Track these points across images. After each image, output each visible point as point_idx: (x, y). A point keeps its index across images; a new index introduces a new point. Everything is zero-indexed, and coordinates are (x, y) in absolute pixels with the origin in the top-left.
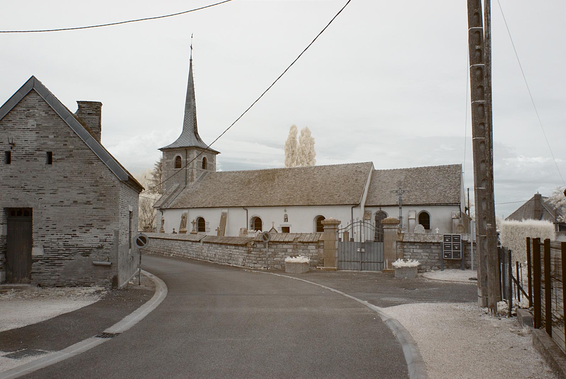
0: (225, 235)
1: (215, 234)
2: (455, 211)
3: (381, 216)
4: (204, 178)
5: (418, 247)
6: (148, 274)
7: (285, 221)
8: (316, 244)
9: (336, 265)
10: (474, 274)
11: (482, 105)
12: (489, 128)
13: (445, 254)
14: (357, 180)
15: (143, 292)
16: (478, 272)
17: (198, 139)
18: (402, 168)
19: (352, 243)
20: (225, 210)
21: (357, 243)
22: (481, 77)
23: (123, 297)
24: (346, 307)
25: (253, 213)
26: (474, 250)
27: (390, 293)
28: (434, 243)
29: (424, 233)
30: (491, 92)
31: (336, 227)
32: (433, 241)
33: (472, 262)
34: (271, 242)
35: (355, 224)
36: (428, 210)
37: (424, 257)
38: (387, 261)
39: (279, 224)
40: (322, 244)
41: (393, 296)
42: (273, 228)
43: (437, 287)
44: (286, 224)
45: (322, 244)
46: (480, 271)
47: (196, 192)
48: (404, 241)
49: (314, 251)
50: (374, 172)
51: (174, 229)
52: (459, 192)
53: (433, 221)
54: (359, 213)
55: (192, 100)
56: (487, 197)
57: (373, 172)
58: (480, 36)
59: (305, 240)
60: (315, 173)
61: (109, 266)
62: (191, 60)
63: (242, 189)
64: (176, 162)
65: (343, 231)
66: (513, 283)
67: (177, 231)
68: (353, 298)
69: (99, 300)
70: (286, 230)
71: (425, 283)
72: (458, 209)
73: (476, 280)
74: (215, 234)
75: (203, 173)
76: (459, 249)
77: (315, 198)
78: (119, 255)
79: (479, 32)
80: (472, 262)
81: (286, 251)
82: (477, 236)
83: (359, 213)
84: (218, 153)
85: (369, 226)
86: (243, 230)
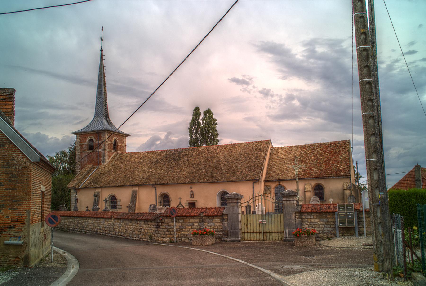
0: (136, 212)
1: (126, 210)
2: (346, 183)
3: (280, 188)
6: (61, 251)
7: (191, 197)
8: (220, 218)
9: (240, 237)
10: (370, 241)
11: (369, 83)
12: (377, 104)
13: (340, 223)
14: (257, 157)
15: (53, 270)
16: (373, 238)
17: (109, 122)
18: (298, 145)
19: (254, 215)
20: (136, 189)
21: (259, 215)
22: (367, 57)
23: (34, 275)
24: (251, 277)
25: (160, 190)
26: (366, 217)
27: (291, 261)
28: (330, 212)
29: (319, 203)
30: (377, 71)
31: (239, 201)
33: (365, 229)
34: (178, 216)
35: (257, 198)
36: (322, 182)
37: (321, 226)
38: (287, 231)
39: (185, 199)
40: (226, 217)
41: (294, 265)
42: (180, 203)
43: (334, 253)
44: (191, 200)
45: (226, 217)
46: (375, 237)
47: (108, 172)
48: (302, 211)
49: (219, 224)
50: (272, 148)
51: (87, 207)
52: (349, 166)
54: (260, 188)
55: (103, 87)
56: (378, 168)
57: (271, 150)
58: (364, 21)
60: (218, 152)
61: (20, 245)
62: (102, 51)
63: (150, 168)
65: (246, 204)
67: (90, 209)
68: (257, 267)
69: (10, 279)
70: (192, 205)
71: (323, 250)
73: (371, 245)
74: (126, 210)
76: (352, 217)
77: (219, 175)
78: (31, 234)
79: (363, 17)
80: (365, 229)
81: (193, 225)
82: (370, 205)
83: (260, 188)
84: (127, 135)
85: (269, 199)
86: (152, 207)
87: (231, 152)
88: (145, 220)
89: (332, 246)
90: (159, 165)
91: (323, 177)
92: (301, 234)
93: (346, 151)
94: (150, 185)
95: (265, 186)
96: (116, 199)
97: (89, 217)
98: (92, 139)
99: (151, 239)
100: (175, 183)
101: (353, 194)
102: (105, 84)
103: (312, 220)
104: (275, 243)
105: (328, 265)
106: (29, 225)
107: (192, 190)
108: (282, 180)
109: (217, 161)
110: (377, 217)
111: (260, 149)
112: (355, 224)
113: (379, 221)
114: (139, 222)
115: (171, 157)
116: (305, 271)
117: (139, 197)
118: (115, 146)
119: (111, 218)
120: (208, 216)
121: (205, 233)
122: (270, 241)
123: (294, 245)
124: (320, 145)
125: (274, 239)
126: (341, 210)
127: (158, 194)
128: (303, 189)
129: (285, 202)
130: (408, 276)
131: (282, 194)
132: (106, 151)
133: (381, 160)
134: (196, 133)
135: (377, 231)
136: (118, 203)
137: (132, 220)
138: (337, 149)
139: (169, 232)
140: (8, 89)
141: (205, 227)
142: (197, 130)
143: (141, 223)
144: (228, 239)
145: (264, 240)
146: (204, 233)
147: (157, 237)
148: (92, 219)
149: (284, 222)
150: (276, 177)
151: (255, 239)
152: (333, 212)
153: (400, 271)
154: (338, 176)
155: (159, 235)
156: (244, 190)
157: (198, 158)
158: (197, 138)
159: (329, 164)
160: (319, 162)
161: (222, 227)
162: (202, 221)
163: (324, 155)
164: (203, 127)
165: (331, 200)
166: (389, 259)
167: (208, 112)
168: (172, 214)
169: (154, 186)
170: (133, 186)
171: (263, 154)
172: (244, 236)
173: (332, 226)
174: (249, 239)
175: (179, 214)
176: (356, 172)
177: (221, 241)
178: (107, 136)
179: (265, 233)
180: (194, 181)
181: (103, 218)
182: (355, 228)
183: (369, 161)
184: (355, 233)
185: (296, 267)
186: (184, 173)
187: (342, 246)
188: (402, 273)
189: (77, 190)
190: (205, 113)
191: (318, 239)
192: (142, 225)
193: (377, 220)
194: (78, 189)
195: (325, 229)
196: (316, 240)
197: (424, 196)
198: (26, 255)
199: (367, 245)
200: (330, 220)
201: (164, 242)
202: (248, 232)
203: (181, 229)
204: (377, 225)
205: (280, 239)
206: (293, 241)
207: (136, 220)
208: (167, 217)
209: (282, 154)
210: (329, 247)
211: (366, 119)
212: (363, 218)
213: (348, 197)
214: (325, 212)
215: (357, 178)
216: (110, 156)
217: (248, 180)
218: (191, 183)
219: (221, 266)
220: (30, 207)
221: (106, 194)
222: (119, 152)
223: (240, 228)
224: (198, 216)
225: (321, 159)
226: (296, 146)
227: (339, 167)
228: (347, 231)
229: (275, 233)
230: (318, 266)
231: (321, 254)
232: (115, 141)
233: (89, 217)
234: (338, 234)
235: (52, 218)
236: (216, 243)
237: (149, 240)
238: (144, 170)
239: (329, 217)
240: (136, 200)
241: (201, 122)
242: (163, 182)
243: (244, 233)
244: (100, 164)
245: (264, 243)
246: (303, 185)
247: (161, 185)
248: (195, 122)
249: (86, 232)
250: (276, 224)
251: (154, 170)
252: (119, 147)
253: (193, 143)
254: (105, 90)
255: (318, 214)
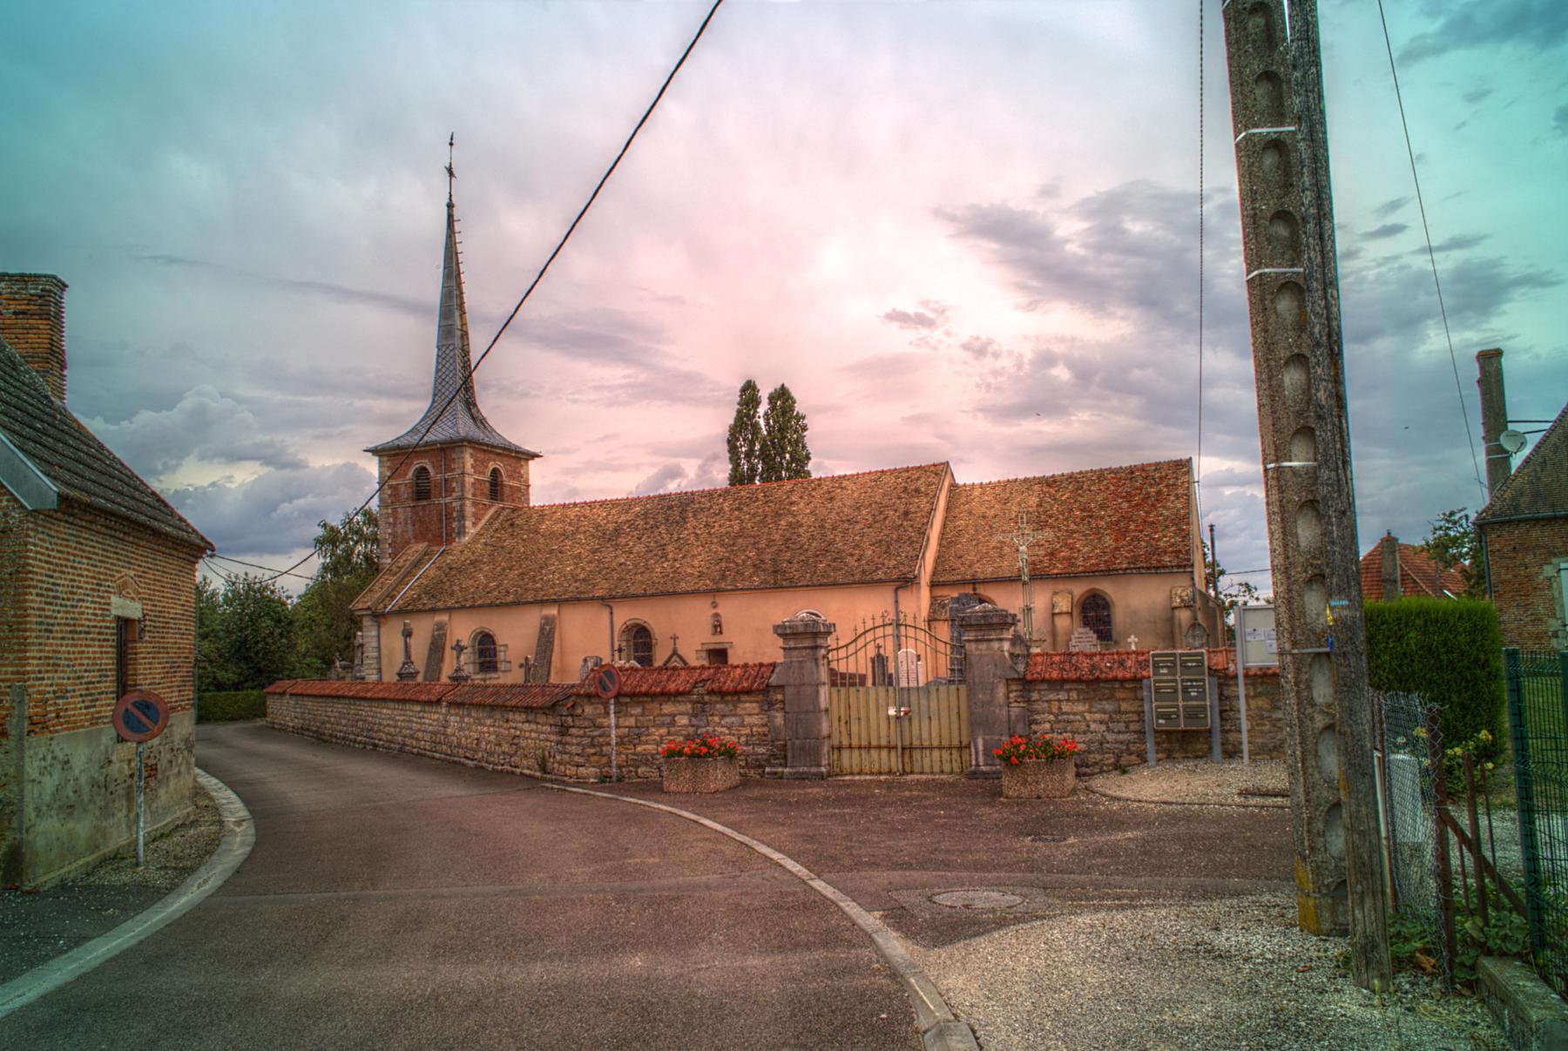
0: (554, 680)
2: (1180, 589)
4: (497, 525)
5: (1074, 695)
7: (715, 633)
8: (760, 697)
9: (824, 762)
14: (906, 513)
20: (552, 611)
25: (625, 615)
26: (1247, 696)
28: (1123, 681)
30: (1317, 64)
31: (820, 642)
32: (1120, 675)
33: (1245, 737)
34: (626, 695)
36: (1107, 587)
37: (1093, 726)
42: (675, 653)
43: (1138, 826)
44: (714, 641)
45: (780, 697)
47: (472, 563)
48: (1029, 677)
49: (755, 720)
50: (954, 486)
52: (1186, 536)
53: (1119, 616)
54: (918, 603)
55: (457, 313)
57: (950, 491)
59: (729, 685)
60: (794, 499)
64: (417, 485)
66: (1454, 854)
70: (719, 655)
71: (1099, 813)
72: (1188, 583)
75: (492, 511)
80: (1245, 737)
81: (673, 723)
84: (534, 456)
86: (590, 665)
87: (831, 499)
88: (528, 709)
89: (1132, 796)
90: (622, 540)
91: (1109, 572)
92: (1023, 756)
93: (1180, 491)
94: (592, 599)
95: (933, 598)
96: (494, 642)
97: (384, 700)
98: (424, 469)
99: (544, 769)
100: (666, 593)
101: (1200, 620)
102: (461, 305)
103: (1065, 707)
104: (940, 786)
105: (1109, 885)
106: (21, 739)
107: (718, 610)
108: (985, 582)
109: (790, 525)
110: (1313, 705)
111: (917, 491)
112: (1212, 719)
113: (1320, 721)
114: (511, 716)
115: (660, 518)
116: (1017, 920)
117: (561, 639)
118: (495, 488)
119: (439, 702)
120: (722, 694)
121: (705, 750)
122: (924, 777)
123: (1001, 794)
124: (1100, 475)
125: (936, 769)
126: (1165, 671)
127: (618, 626)
128: (1040, 609)
129: (973, 646)
130: (1462, 974)
131: (963, 619)
132: (468, 503)
133: (1336, 458)
134: (749, 455)
135: (1311, 762)
136: (501, 656)
137: (493, 708)
138: (1151, 485)
139: (597, 743)
140: (35, 276)
141: (710, 729)
142: (752, 444)
143: (517, 717)
144: (787, 770)
145: (904, 773)
146: (703, 752)
147: (560, 763)
148: (392, 705)
149: (971, 714)
150: (965, 572)
151: (876, 768)
152: (1136, 680)
153: (1418, 945)
154: (1151, 566)
155: (566, 757)
156: (853, 615)
157: (738, 518)
158: (752, 469)
159: (1127, 530)
160: (1097, 527)
161: (765, 729)
162: (700, 710)
163: (1112, 504)
164: (768, 435)
165: (1132, 639)
166: (1374, 896)
167: (782, 397)
168: (605, 689)
169: (607, 601)
170: (543, 603)
171: (923, 503)
172: (839, 758)
173: (1133, 727)
174: (856, 769)
175: (627, 689)
176: (1209, 559)
177: (762, 775)
178: (469, 461)
179: (907, 749)
180: (723, 585)
181: (417, 702)
182: (1210, 731)
183: (1277, 469)
184: (1210, 749)
185: (988, 899)
186: (696, 563)
187: (1165, 798)
188: (1426, 952)
189: (379, 617)
190: (772, 399)
191: (1084, 770)
192: (520, 724)
193: (1312, 719)
194: (383, 615)
195: (1110, 737)
196: (1078, 775)
197: (1452, 621)
198: (9, 847)
199: (1254, 794)
200: (1124, 706)
201: (581, 782)
202: (850, 747)
203: (631, 738)
204: (1310, 741)
205: (956, 769)
206: (997, 776)
207: (505, 708)
208: (589, 696)
209: (982, 503)
210: (1119, 799)
211: (1262, 292)
212: (1237, 697)
213: (1184, 630)
214: (1107, 681)
215: (1212, 575)
216: (477, 518)
217: (880, 581)
218: (714, 592)
219: (708, 887)
220: (24, 673)
221: (462, 629)
222: (507, 504)
223: (825, 732)
224: (689, 693)
225: (1102, 518)
226: (1026, 480)
227: (1159, 540)
228: (1185, 744)
229: (940, 748)
230: (1069, 889)
231: (1093, 828)
232: (495, 472)
233: (384, 700)
234: (1152, 756)
235: (136, 711)
236: (745, 783)
237: (538, 774)
238: (579, 556)
239: (1122, 695)
240: (552, 643)
241: (762, 422)
242: (632, 590)
243: (840, 748)
244: (449, 541)
245: (903, 786)
246: (1048, 594)
247: (627, 597)
248: (743, 424)
249: (375, 746)
250: (944, 721)
251: (608, 554)
252: (507, 491)
253: (737, 479)
254: (464, 324)
255: (1084, 686)
